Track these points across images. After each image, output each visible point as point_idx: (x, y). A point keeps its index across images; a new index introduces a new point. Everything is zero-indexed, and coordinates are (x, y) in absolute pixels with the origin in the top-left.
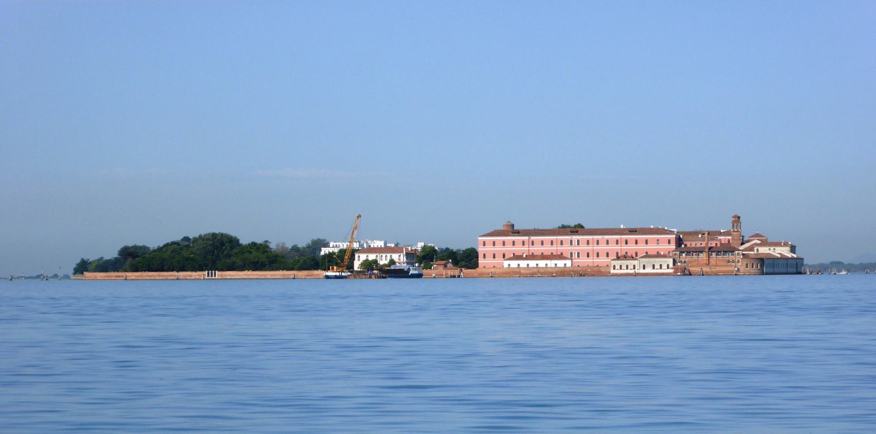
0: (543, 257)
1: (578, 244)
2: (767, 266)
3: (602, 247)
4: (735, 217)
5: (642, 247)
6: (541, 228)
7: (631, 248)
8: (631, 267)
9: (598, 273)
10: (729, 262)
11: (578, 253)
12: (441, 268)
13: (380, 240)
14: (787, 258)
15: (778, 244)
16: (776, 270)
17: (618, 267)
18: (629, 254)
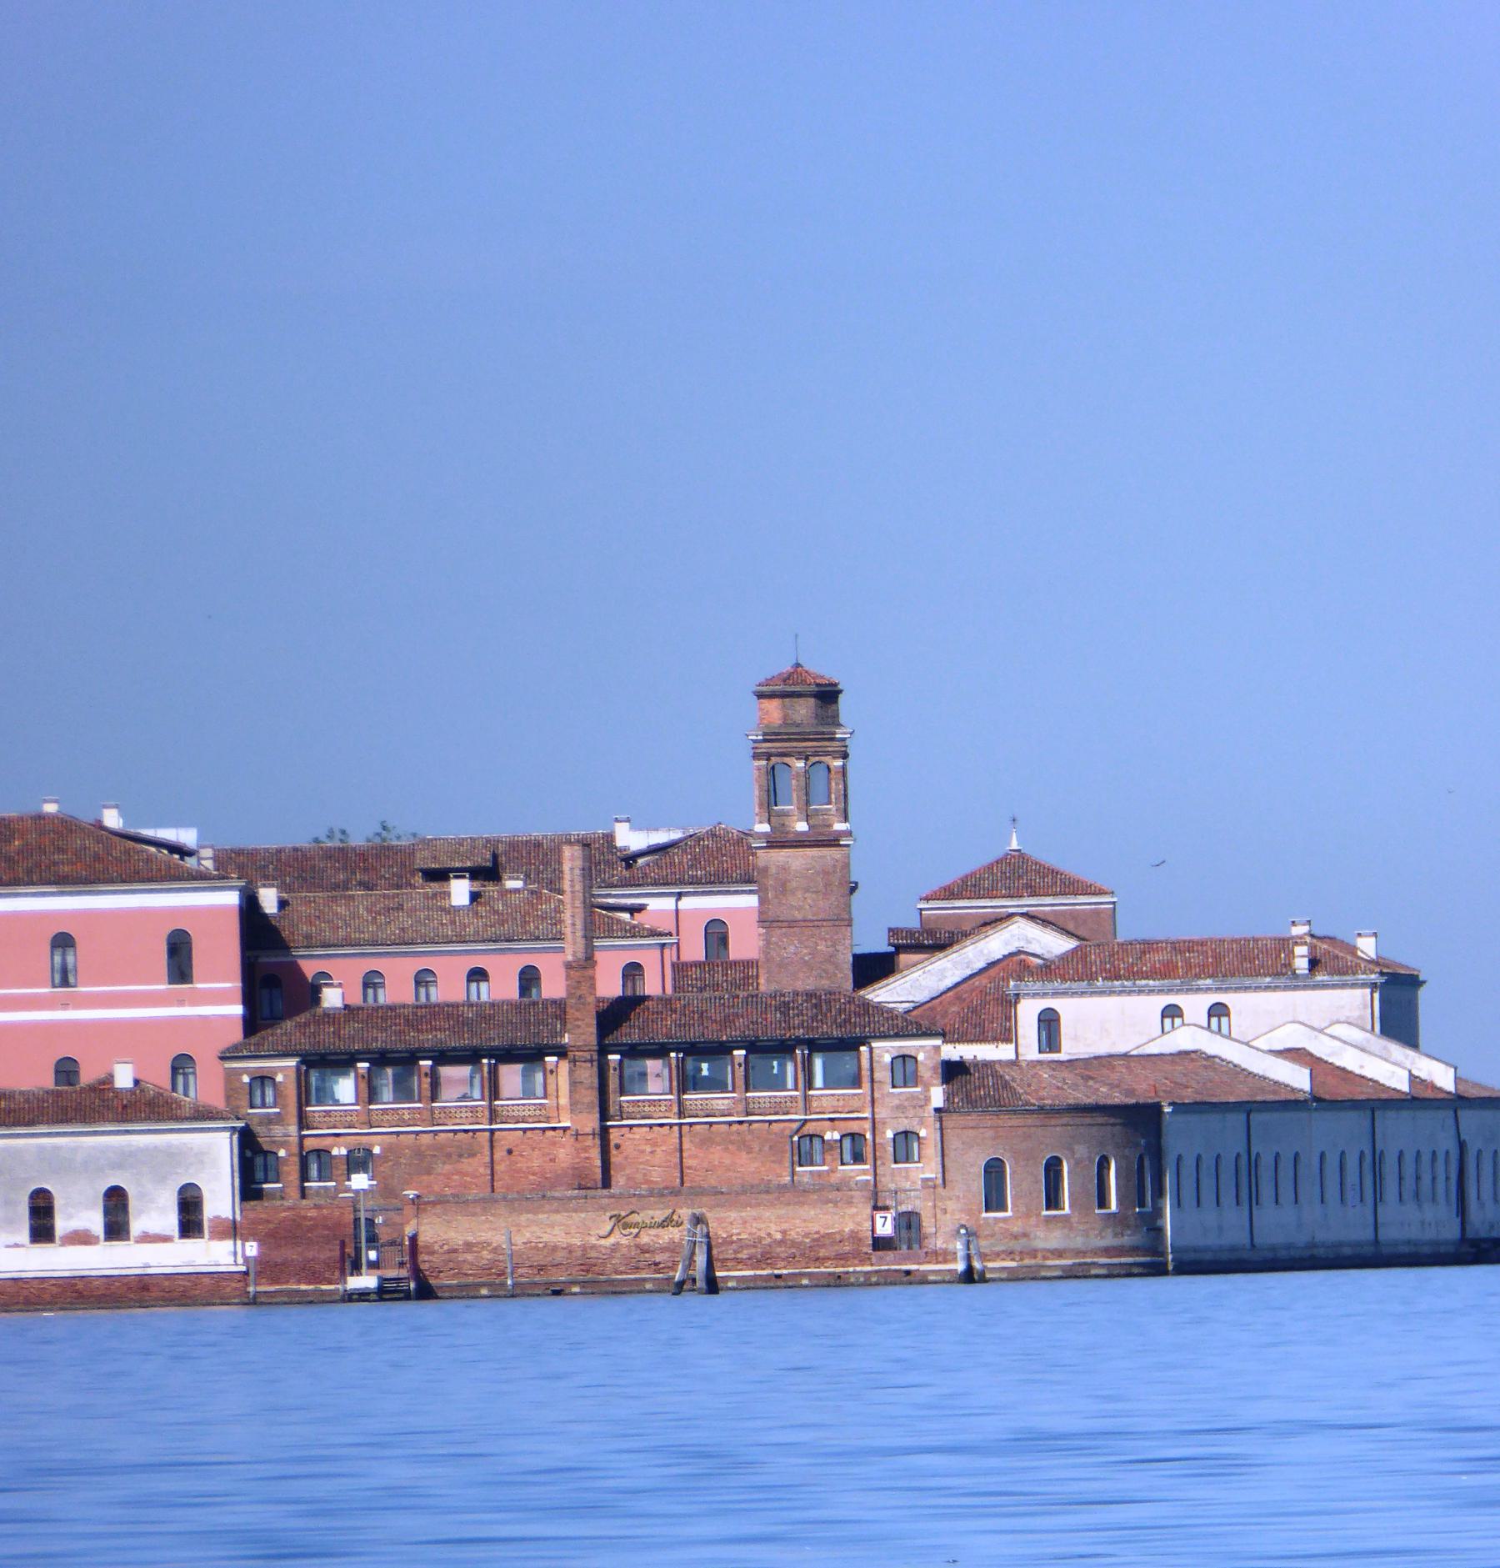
4: (784, 688)
10: (805, 1146)
14: (1380, 1105)
15: (1256, 962)
16: (1277, 1224)
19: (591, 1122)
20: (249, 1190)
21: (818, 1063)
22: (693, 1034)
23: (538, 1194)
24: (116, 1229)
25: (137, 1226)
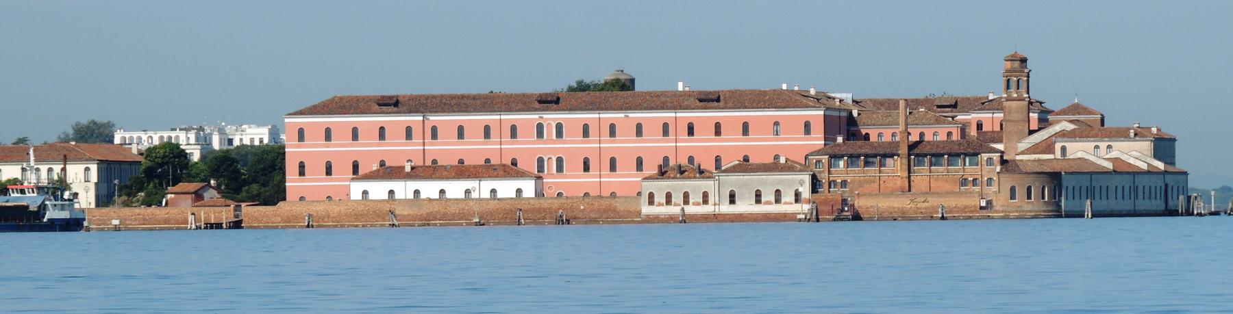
0: (461, 171)
1: (559, 134)
2: (1064, 193)
3: (625, 145)
4: (1011, 59)
5: (732, 145)
6: (509, 92)
7: (703, 146)
8: (696, 197)
9: (606, 214)
10: (964, 182)
11: (560, 161)
12: (186, 203)
13: (260, 125)
17: (660, 198)
18: (521, 165)
19: (906, 174)
20: (814, 190)
21: (967, 159)
22: (933, 151)
23: (891, 194)
24: (778, 201)
25: (763, 199)
